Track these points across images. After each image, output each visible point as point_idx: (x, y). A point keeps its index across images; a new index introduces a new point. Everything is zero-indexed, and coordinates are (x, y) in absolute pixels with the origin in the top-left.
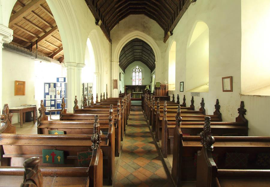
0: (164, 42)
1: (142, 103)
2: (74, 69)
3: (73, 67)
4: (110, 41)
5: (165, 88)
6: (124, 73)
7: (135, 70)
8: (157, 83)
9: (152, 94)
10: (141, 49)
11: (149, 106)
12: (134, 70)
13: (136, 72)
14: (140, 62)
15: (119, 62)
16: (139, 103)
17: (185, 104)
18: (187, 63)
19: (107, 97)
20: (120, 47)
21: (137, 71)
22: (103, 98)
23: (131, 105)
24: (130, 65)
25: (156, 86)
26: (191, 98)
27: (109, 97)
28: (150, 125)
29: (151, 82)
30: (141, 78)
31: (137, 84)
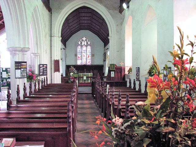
0: (119, 12)
1: (92, 90)
2: (19, 54)
3: (17, 53)
4: (50, 10)
5: (121, 70)
6: (65, 48)
7: (81, 43)
8: (111, 65)
9: (106, 77)
10: (90, 16)
11: (101, 93)
12: (79, 43)
13: (82, 46)
14: (88, 32)
15: (61, 37)
16: (88, 90)
17: (140, 89)
18: (137, 47)
19: (47, 83)
20: (62, 18)
21: (84, 44)
22: (43, 84)
23: (79, 93)
24: (74, 36)
25: (110, 69)
26: (145, 83)
27: (49, 82)
28: (102, 112)
29: (105, 61)
30: (89, 53)
31: (84, 63)
